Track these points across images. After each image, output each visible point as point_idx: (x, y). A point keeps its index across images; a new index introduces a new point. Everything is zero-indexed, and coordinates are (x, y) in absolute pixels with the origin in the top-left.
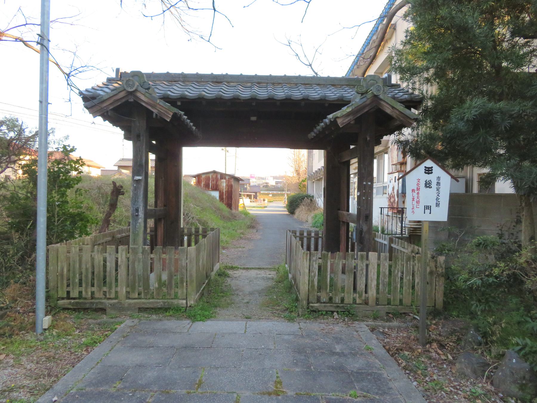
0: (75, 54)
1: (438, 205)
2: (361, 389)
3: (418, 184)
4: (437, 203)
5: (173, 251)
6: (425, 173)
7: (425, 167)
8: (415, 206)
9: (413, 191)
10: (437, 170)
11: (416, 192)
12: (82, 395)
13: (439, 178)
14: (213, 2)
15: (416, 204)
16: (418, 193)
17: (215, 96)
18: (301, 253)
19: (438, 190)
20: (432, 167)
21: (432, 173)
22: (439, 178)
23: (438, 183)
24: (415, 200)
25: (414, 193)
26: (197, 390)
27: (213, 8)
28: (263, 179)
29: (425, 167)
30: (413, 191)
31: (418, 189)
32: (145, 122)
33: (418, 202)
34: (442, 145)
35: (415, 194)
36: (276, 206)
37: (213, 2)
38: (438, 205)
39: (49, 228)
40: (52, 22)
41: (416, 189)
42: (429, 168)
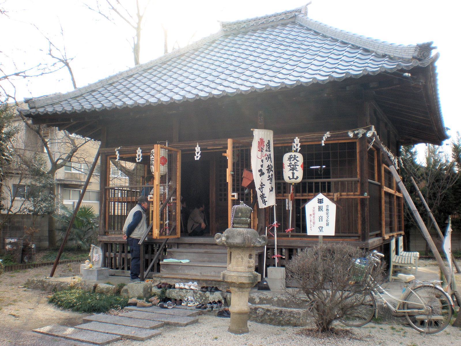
1: (327, 225)
3: (314, 211)
5: (35, 299)
6: (318, 203)
7: (318, 199)
9: (310, 215)
10: (326, 201)
11: (313, 216)
14: (137, 2)
15: (313, 224)
16: (314, 217)
17: (135, 281)
19: (327, 214)
20: (322, 199)
21: (322, 203)
23: (327, 209)
24: (312, 221)
25: (311, 217)
27: (136, 26)
29: (318, 199)
31: (314, 214)
33: (314, 223)
34: (9, 249)
35: (312, 217)
37: (137, 2)
38: (327, 225)
39: (372, 180)
41: (312, 214)
42: (320, 199)
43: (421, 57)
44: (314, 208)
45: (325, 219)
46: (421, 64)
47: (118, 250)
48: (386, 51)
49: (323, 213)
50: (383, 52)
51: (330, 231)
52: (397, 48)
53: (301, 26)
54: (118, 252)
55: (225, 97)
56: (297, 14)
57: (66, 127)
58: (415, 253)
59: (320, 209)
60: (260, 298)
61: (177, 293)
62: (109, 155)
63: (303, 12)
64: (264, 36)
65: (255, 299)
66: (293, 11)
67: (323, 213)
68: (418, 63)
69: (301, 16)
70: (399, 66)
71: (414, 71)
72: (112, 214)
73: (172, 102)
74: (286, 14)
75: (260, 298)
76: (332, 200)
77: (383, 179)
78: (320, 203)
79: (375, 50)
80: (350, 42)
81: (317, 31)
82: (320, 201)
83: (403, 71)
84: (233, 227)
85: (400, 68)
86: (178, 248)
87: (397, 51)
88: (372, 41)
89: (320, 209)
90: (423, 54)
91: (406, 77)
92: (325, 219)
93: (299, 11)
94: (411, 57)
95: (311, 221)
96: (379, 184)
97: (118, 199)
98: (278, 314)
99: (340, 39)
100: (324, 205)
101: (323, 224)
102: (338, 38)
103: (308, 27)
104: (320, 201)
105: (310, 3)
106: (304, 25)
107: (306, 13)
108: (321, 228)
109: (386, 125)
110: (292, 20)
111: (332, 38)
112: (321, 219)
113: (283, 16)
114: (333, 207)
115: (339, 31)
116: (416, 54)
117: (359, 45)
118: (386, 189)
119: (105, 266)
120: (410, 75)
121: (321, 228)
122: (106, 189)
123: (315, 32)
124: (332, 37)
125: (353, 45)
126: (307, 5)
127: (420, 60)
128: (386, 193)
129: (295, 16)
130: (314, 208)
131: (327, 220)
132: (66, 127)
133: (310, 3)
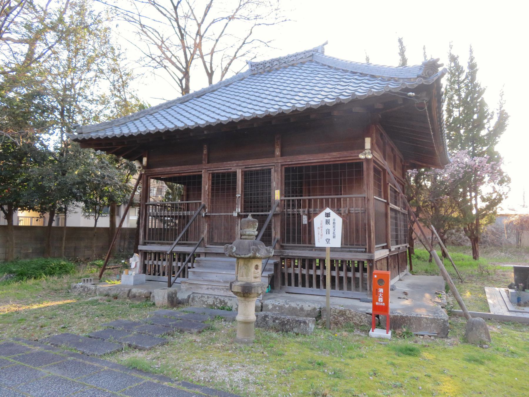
0: (140, 15)
1: (334, 237)
2: (475, 294)
4: (333, 236)
8: (320, 238)
9: (319, 228)
11: (320, 229)
12: (481, 299)
13: (334, 220)
16: (322, 230)
18: (129, 289)
19: (334, 227)
21: (330, 216)
22: (334, 220)
23: (334, 223)
24: (320, 234)
26: (277, 361)
28: (513, 210)
30: (319, 228)
31: (322, 227)
32: (393, 163)
33: (322, 235)
35: (320, 230)
36: (370, 230)
38: (334, 237)
40: (404, 61)
42: (328, 213)
43: (426, 75)
44: (322, 221)
45: (331, 232)
46: (425, 82)
47: (296, 264)
48: (391, 74)
49: (330, 227)
50: (388, 76)
51: (337, 243)
52: (402, 70)
53: (317, 62)
54: (297, 267)
55: (243, 121)
56: (314, 53)
57: (113, 151)
58: (178, 185)
59: (327, 222)
60: (273, 305)
61: (199, 298)
62: (149, 176)
63: (320, 51)
64: (285, 72)
65: (268, 305)
66: (311, 51)
67: (330, 227)
68: (423, 81)
69: (317, 54)
70: (403, 85)
71: (419, 89)
72: (162, 227)
73: (197, 126)
74: (305, 54)
75: (273, 305)
76: (339, 214)
77: (389, 196)
78: (328, 217)
79: (381, 75)
80: (358, 71)
81: (330, 65)
82: (328, 215)
83: (408, 90)
84: (241, 239)
85: (404, 87)
86: (205, 256)
87: (402, 73)
88: (379, 67)
89: (327, 222)
90: (428, 73)
91: (410, 97)
92: (331, 232)
93: (316, 50)
94: (416, 77)
95: (319, 233)
96: (385, 201)
97: (153, 214)
98: (286, 322)
99: (350, 70)
100: (331, 219)
101: (330, 236)
102: (348, 69)
103: (323, 63)
104: (328, 215)
105: (326, 43)
106: (320, 62)
107: (323, 52)
108: (328, 241)
109: (392, 150)
110: (310, 58)
111: (343, 70)
112: (328, 232)
113: (303, 56)
114: (339, 221)
115: (349, 62)
116: (420, 73)
117: (366, 73)
118: (392, 206)
119: (145, 272)
120: (414, 94)
121: (328, 241)
122: (146, 206)
123: (329, 67)
124: (343, 68)
125: (361, 74)
126: (324, 45)
127: (424, 78)
128: (392, 209)
129: (312, 55)
130: (322, 221)
131: (334, 233)
132: (113, 151)
133: (326, 43)
